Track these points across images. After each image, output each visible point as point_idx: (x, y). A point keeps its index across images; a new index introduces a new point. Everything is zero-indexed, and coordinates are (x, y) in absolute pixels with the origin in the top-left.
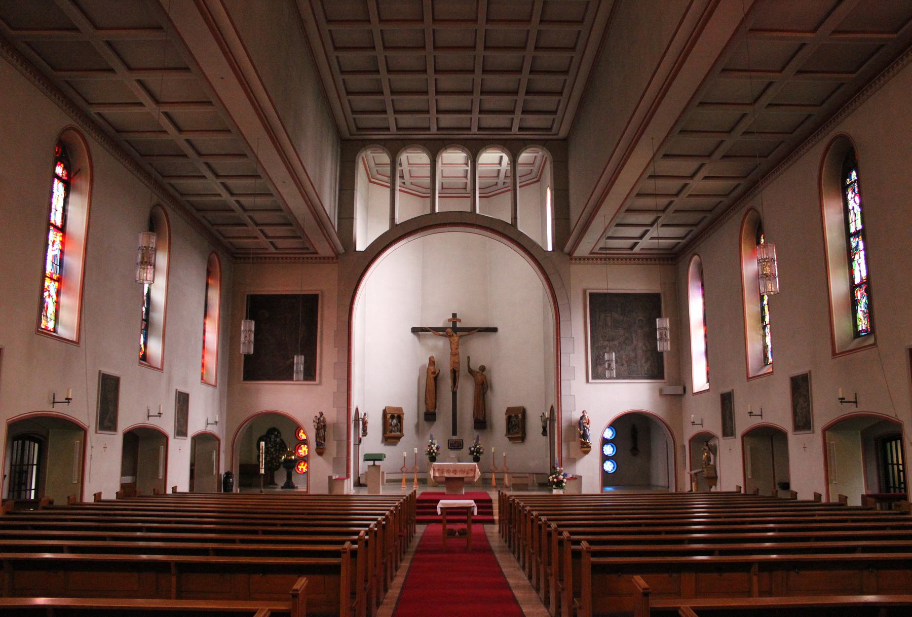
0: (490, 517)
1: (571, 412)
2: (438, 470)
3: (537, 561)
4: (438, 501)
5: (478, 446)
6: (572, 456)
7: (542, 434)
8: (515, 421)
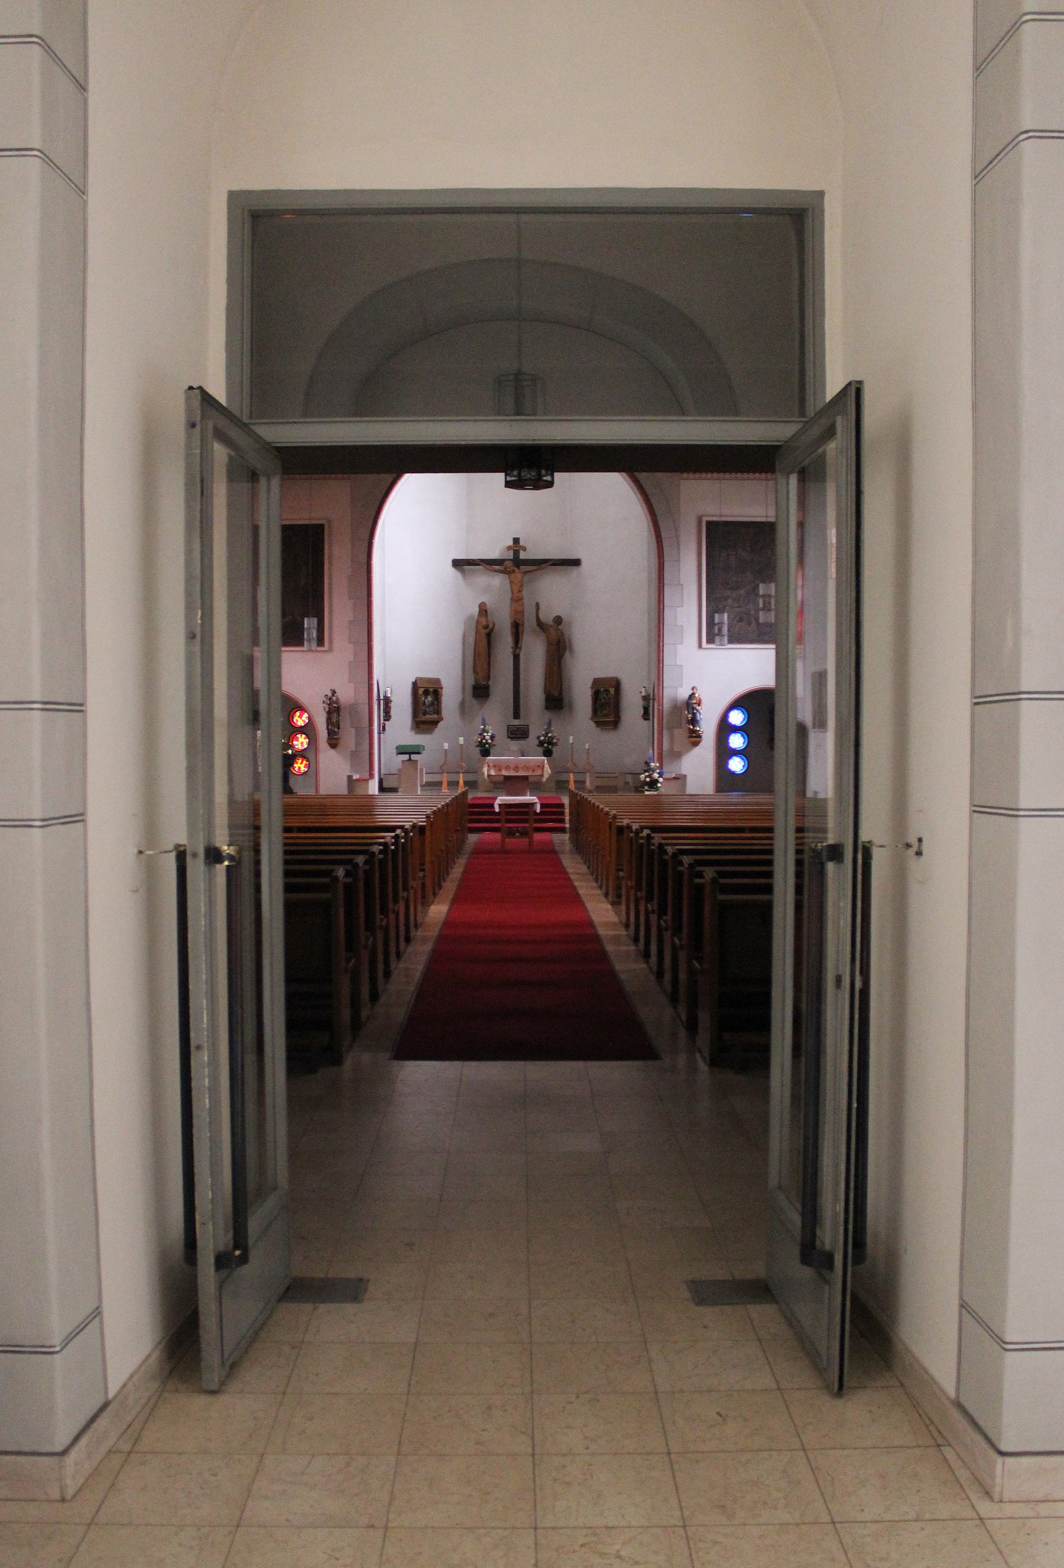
0: (562, 825)
1: (676, 689)
2: (494, 766)
3: (673, 942)
4: (495, 799)
5: (550, 735)
6: (676, 749)
7: (642, 717)
8: (604, 698)
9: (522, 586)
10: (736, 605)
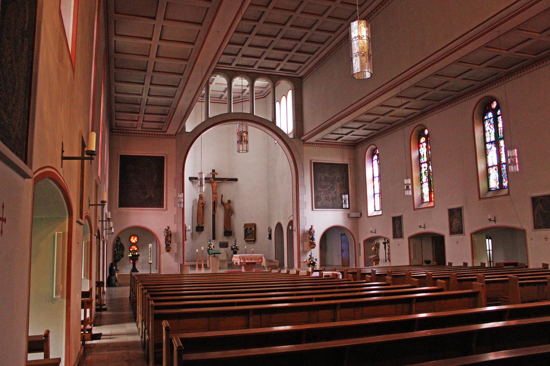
2: (242, 258)
6: (305, 250)
9: (216, 188)
10: (324, 194)
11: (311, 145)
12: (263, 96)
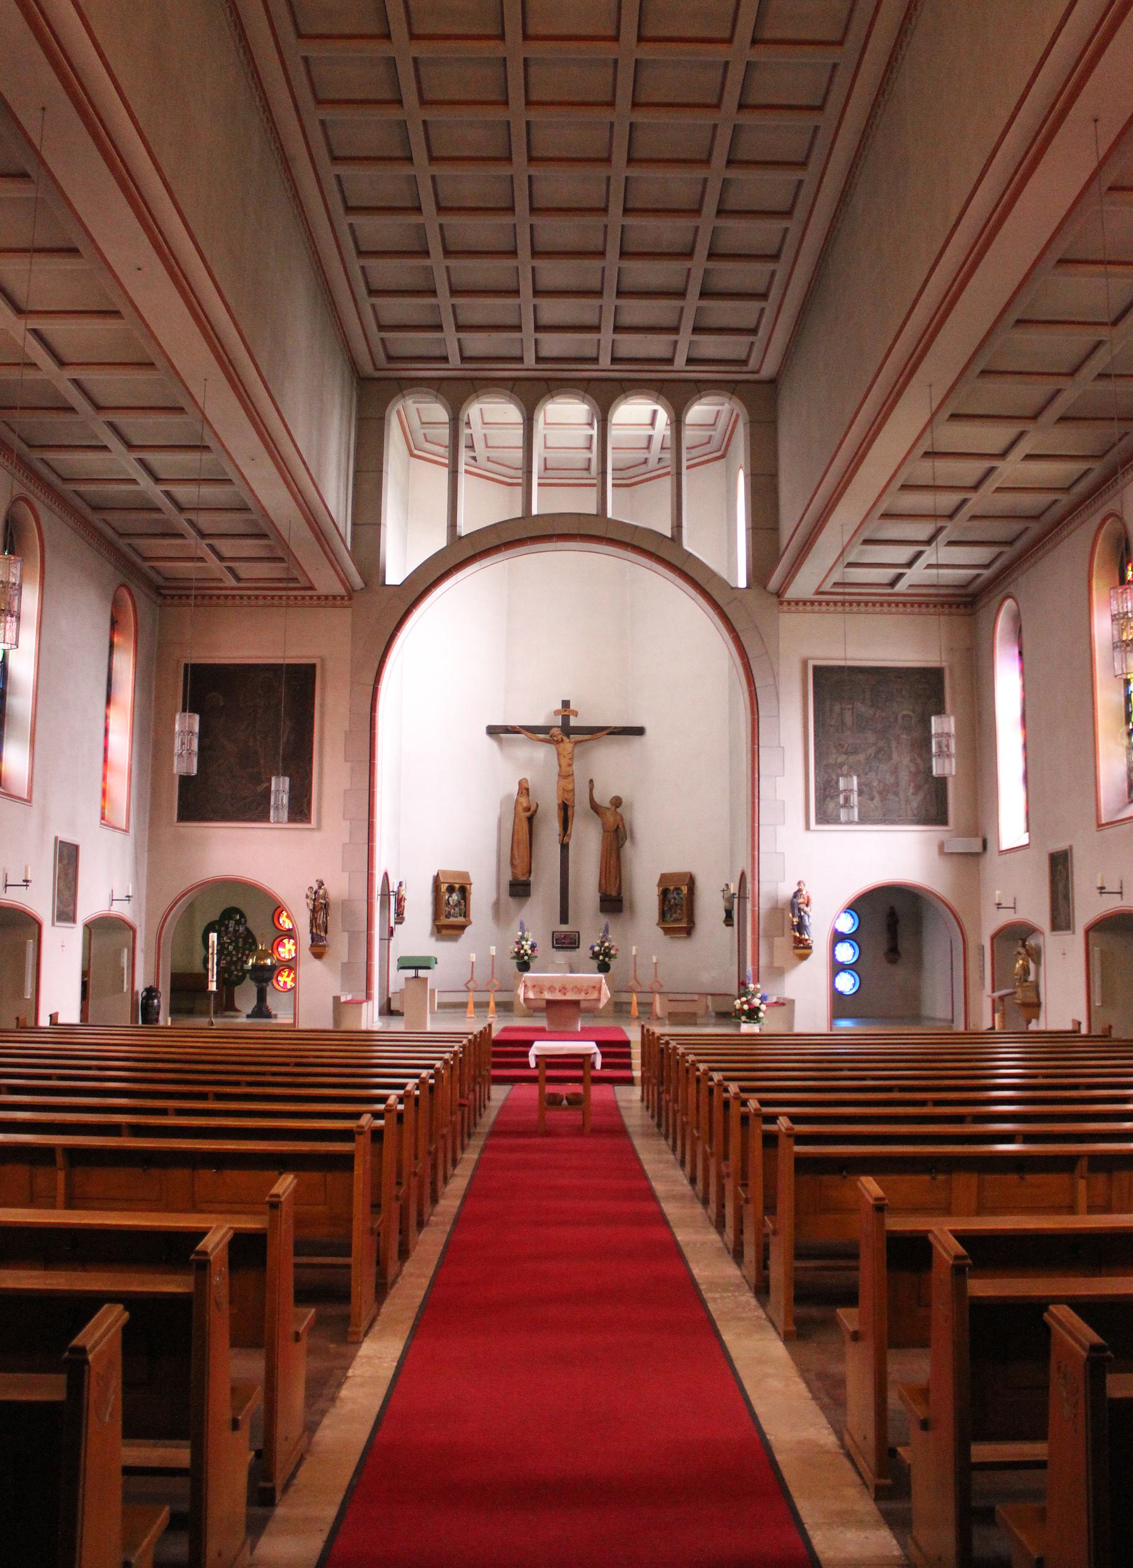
4: (530, 1043)
5: (606, 944)
7: (725, 922)
8: (675, 898)
9: (571, 759)
11: (801, 608)
12: (714, 455)
